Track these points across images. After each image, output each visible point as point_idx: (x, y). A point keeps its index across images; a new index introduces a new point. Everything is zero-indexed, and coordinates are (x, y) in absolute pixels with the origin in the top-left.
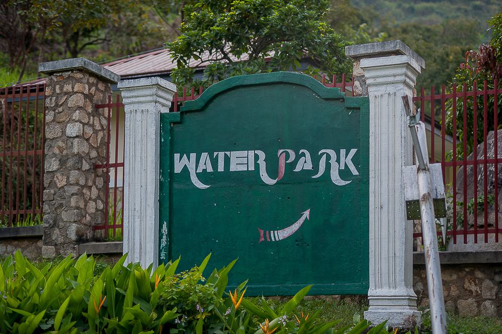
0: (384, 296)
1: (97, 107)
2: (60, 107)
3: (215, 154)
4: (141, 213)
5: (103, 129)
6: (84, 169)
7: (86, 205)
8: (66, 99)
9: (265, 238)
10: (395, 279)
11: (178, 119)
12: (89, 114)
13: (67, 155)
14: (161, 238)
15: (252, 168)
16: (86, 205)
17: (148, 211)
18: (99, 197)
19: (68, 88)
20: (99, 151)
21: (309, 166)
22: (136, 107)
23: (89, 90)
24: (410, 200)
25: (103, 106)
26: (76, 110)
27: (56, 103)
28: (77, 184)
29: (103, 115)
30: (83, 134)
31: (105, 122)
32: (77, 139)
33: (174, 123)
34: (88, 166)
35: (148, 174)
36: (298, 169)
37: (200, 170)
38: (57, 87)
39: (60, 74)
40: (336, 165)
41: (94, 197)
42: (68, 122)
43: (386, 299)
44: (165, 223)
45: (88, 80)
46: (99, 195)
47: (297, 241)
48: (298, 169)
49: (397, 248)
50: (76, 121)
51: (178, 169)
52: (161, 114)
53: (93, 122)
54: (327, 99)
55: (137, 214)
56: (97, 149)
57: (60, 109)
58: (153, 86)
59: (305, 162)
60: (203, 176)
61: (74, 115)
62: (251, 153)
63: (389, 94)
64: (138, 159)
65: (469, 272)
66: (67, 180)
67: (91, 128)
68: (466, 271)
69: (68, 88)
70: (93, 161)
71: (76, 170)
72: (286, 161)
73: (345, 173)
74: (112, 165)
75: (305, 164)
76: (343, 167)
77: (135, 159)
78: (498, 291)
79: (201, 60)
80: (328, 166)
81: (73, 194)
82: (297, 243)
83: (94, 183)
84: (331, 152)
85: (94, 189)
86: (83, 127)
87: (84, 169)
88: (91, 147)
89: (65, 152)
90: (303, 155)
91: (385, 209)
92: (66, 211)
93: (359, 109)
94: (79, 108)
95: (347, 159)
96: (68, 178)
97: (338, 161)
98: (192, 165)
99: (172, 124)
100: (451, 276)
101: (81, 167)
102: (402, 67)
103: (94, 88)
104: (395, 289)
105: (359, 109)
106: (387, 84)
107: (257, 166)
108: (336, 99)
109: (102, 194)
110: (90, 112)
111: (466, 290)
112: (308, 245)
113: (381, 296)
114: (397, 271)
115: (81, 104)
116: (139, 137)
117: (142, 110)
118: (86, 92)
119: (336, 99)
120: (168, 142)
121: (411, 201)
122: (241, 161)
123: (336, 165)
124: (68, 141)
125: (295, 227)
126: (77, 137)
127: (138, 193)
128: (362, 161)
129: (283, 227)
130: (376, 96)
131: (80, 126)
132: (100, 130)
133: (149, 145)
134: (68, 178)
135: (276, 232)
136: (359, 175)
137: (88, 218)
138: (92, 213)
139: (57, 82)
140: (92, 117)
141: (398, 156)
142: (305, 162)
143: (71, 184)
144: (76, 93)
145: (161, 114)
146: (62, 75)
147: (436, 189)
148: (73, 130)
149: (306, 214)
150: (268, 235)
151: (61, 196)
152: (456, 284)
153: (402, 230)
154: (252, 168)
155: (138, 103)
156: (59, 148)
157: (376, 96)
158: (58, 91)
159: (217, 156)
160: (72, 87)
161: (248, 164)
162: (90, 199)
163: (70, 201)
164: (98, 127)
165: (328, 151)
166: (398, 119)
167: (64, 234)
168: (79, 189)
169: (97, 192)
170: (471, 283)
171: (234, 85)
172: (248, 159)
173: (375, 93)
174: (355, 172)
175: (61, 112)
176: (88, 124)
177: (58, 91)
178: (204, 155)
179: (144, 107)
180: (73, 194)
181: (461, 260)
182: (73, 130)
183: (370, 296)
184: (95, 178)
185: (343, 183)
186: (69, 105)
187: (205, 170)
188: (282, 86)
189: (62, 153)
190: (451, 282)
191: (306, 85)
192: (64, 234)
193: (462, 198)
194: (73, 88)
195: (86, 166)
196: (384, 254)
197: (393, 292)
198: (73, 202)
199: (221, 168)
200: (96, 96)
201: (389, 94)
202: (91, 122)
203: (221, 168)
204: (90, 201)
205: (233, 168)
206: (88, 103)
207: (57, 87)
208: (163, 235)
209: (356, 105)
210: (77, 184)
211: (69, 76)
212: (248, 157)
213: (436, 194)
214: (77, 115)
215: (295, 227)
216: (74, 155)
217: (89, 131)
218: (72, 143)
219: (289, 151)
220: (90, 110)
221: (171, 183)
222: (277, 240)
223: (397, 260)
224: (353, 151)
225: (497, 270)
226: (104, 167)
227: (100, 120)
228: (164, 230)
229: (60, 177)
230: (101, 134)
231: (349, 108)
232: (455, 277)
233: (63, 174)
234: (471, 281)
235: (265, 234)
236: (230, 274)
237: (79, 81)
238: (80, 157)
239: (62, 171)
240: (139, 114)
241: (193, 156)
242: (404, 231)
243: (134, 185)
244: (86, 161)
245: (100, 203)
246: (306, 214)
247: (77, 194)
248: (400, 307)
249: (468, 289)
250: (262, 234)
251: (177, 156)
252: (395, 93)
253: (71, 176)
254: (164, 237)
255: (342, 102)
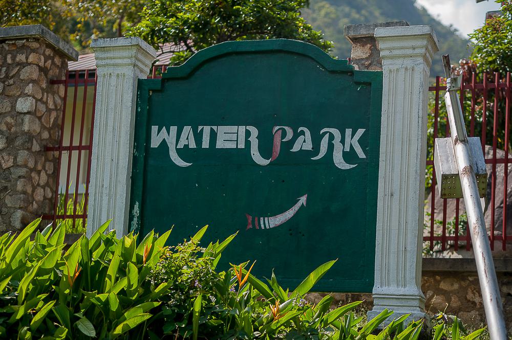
0: (391, 295)
1: (52, 82)
2: (11, 79)
3: (200, 128)
4: (110, 190)
5: (56, 109)
6: (34, 150)
7: (33, 191)
8: (18, 70)
9: (254, 225)
10: (404, 277)
11: (159, 87)
12: (42, 89)
13: (16, 132)
14: (131, 218)
15: (242, 145)
16: (33, 191)
17: (119, 188)
18: (47, 184)
19: (21, 58)
20: (52, 132)
21: (308, 146)
22: (111, 70)
23: (45, 62)
24: (447, 173)
25: (59, 82)
26: (29, 83)
27: (6, 74)
28: (26, 166)
29: (58, 93)
30: (35, 110)
31: (59, 101)
32: (28, 116)
33: (154, 91)
34: (38, 146)
35: (121, 146)
36: (296, 148)
37: (180, 146)
38: (9, 56)
39: (13, 42)
40: (340, 146)
41: (42, 183)
42: (19, 96)
43: (393, 298)
44: (137, 203)
45: (45, 51)
46: (48, 182)
47: (290, 230)
48: (296, 148)
49: (409, 241)
50: (29, 96)
51: (155, 143)
52: (139, 80)
53: (47, 99)
54: (333, 72)
55: (106, 191)
56: (49, 130)
57: (11, 82)
58: (133, 47)
59: (304, 141)
60: (184, 153)
61: (27, 88)
62: (242, 129)
63: (406, 69)
64: (110, 128)
65: (473, 281)
66: (14, 161)
67: (44, 106)
68: (469, 280)
69: (21, 58)
70: (44, 143)
71: (25, 149)
72: (282, 139)
73: (349, 156)
74: (66, 148)
75: (304, 143)
76: (347, 149)
77: (106, 129)
78: (505, 304)
79: (162, 51)
80: (331, 147)
81: (20, 177)
82: (291, 232)
83: (44, 167)
84: (336, 132)
85: (43, 174)
86: (36, 103)
87: (34, 150)
88: (43, 127)
89: (13, 130)
90: (303, 133)
91: (396, 196)
92: (10, 195)
93: (370, 84)
94: (33, 81)
95: (354, 139)
96: (15, 159)
97: (343, 141)
98: (172, 139)
99: (151, 92)
100: (452, 285)
101: (31, 148)
102: (423, 39)
103: (50, 62)
104: (404, 287)
105: (370, 84)
106: (405, 56)
107: (248, 143)
108: (343, 72)
109: (51, 180)
110: (45, 87)
111: (469, 301)
112: (303, 235)
113: (388, 295)
114: (408, 267)
115: (35, 76)
116: (112, 105)
117: (118, 75)
118: (41, 64)
119: (343, 72)
120: (146, 112)
121: (448, 175)
122: (230, 137)
123: (340, 146)
124: (18, 117)
125: (290, 214)
126: (29, 113)
127: (108, 168)
128: (372, 142)
129: (274, 214)
130: (390, 71)
131: (32, 100)
132: (53, 110)
133: (124, 113)
134: (15, 159)
135: (266, 219)
136: (367, 159)
137: (35, 206)
138: (39, 201)
139: (9, 50)
140: (45, 93)
141: (414, 139)
142: (304, 141)
143: (18, 166)
144: (30, 64)
145: (139, 80)
146: (15, 43)
147: (477, 164)
148: (24, 105)
149: (303, 200)
150: (256, 222)
151: (6, 179)
152: (457, 294)
153: (415, 221)
154: (242, 145)
155: (114, 65)
156: (7, 124)
157: (390, 71)
158: (9, 61)
159: (202, 130)
160: (26, 57)
161: (237, 141)
162: (38, 185)
163: (16, 184)
164: (51, 106)
165: (332, 130)
166: (415, 97)
167: (7, 222)
168: (27, 172)
169: (47, 179)
170: (474, 294)
171: (225, 51)
172: (237, 135)
173: (390, 66)
174: (361, 155)
175: (11, 85)
176: (41, 100)
177: (9, 61)
178: (187, 129)
179: (120, 71)
180: (20, 177)
181: (465, 267)
182: (24, 105)
183: (375, 295)
184: (45, 161)
185: (348, 167)
186: (21, 77)
187: (186, 146)
188: (282, 55)
189: (10, 130)
190: (451, 292)
191: (310, 55)
192: (7, 222)
193: (442, 215)
194: (27, 58)
195: (36, 147)
196: (393, 248)
197: (402, 291)
198: (20, 186)
199: (206, 144)
200: (51, 71)
201: (406, 69)
202: (45, 99)
203: (206, 144)
204: (38, 188)
205: (220, 144)
206: (43, 76)
207: (9, 56)
208: (133, 216)
209: (366, 80)
210: (26, 166)
211: (23, 45)
212: (237, 133)
213: (477, 170)
214: (29, 89)
215: (290, 214)
216: (24, 133)
217: (42, 108)
218: (22, 120)
219: (286, 128)
220: (44, 86)
221: (146, 158)
222: (267, 227)
223: (408, 255)
224: (361, 132)
225: (505, 280)
226: (57, 150)
227: (54, 98)
228: (135, 212)
229: (6, 157)
230: (54, 115)
231: (358, 84)
232: (456, 286)
233: (9, 154)
234: (475, 291)
235: (253, 221)
236: (225, 252)
237: (34, 51)
238: (30, 137)
239: (8, 151)
240: (114, 78)
241: (174, 129)
242: (417, 222)
243: (104, 159)
244: (37, 141)
245: (48, 190)
246: (303, 200)
247: (24, 177)
248: (409, 308)
249: (471, 300)
250: (250, 220)
251: (155, 128)
252: (413, 67)
253: (19, 157)
254: (135, 219)
255: (351, 75)
